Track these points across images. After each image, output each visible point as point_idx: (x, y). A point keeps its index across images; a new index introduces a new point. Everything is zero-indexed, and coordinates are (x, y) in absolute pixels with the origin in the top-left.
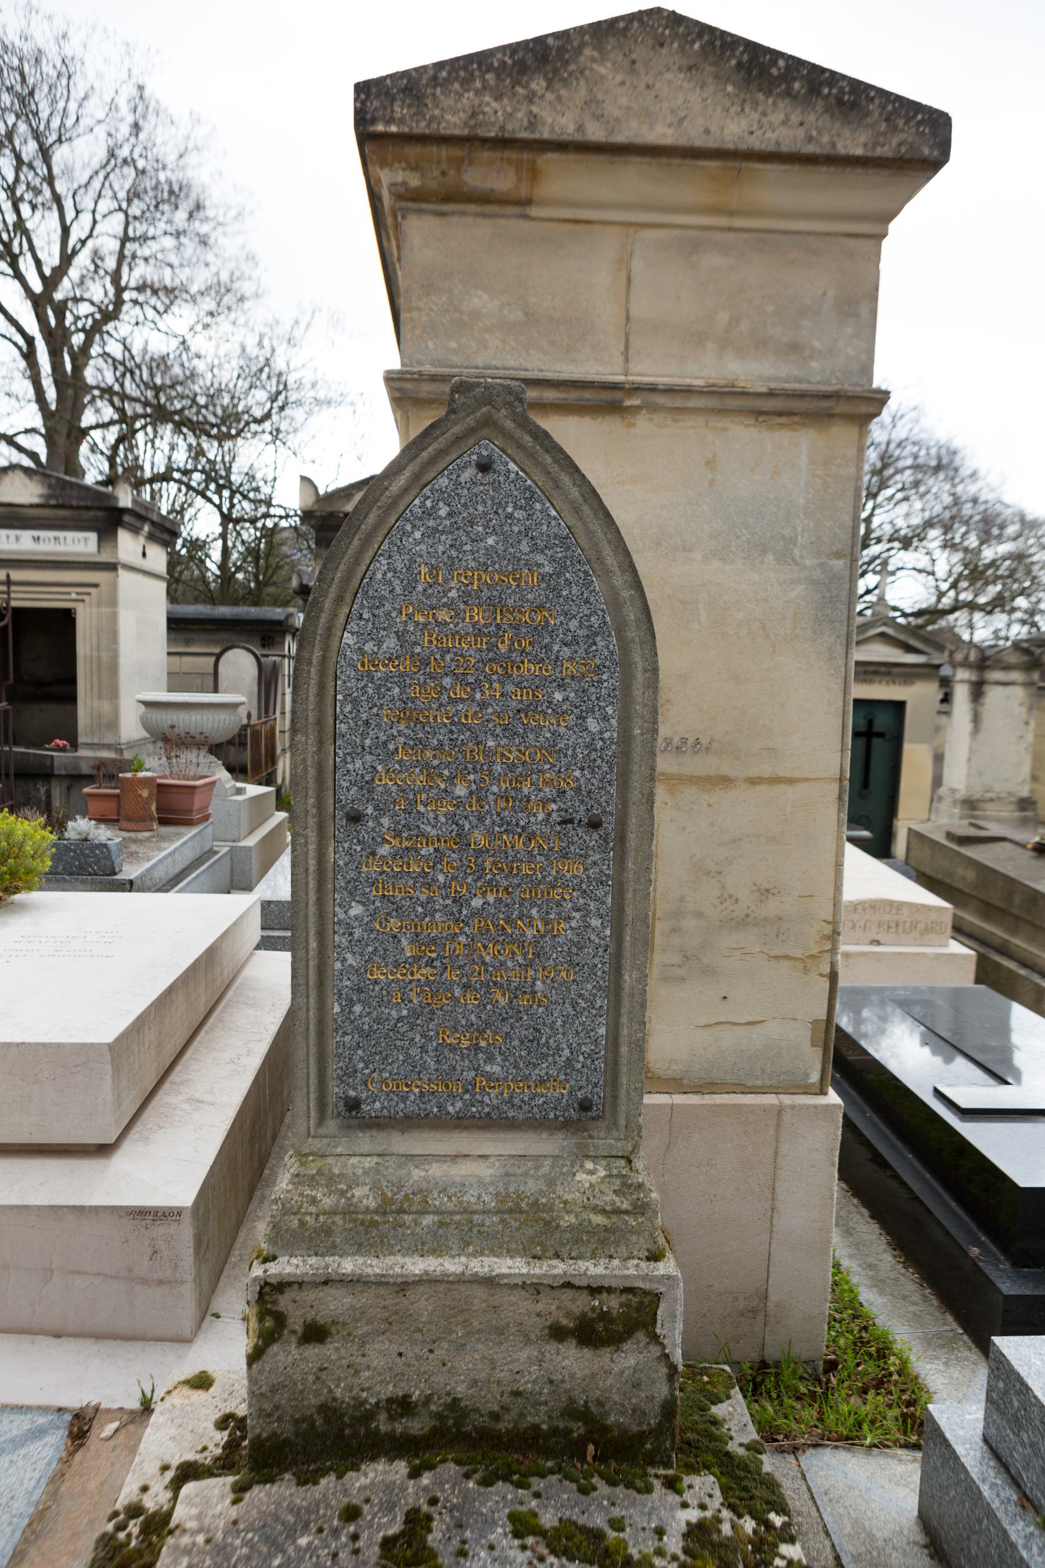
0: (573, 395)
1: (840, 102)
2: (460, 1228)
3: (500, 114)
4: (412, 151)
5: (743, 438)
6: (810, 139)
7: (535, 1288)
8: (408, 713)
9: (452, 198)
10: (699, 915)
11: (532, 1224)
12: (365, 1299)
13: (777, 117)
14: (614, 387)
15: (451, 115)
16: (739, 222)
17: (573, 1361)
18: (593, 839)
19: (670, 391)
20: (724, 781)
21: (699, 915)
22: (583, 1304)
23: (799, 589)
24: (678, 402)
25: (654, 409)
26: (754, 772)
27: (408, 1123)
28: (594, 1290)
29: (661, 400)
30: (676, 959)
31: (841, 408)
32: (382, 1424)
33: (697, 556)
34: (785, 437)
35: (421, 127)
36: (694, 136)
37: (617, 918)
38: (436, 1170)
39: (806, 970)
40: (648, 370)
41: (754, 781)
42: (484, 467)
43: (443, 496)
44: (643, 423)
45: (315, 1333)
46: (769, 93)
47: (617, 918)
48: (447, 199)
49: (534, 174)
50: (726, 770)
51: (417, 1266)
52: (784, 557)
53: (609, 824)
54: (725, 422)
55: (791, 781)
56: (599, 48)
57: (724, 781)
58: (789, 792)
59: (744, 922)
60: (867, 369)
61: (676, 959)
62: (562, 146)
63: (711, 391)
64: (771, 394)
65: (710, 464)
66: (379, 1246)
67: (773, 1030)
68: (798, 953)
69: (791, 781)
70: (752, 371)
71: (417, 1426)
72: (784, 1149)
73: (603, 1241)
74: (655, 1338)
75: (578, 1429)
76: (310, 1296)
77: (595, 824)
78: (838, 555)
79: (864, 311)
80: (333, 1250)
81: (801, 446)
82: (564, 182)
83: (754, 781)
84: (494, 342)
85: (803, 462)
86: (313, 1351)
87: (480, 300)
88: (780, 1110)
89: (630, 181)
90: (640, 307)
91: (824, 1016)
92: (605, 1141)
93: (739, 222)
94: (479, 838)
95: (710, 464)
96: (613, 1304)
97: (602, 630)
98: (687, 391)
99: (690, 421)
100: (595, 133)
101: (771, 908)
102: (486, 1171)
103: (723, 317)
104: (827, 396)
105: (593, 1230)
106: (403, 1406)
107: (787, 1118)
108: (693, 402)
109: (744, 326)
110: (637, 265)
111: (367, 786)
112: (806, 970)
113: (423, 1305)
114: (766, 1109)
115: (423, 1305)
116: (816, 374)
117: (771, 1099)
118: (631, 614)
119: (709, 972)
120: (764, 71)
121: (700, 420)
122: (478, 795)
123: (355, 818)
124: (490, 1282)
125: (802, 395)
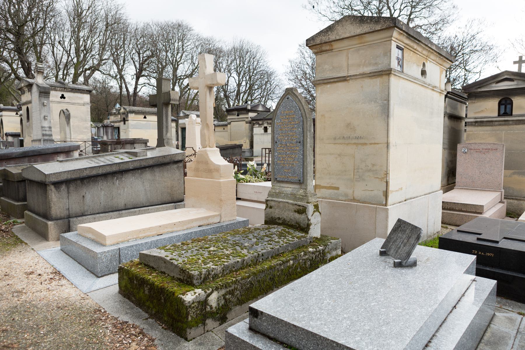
0: (339, 79)
1: (376, 21)
2: (286, 196)
3: (324, 39)
4: (314, 47)
5: (368, 82)
6: (371, 29)
7: (293, 204)
8: (281, 130)
9: (322, 52)
10: (362, 169)
11: (293, 196)
12: (276, 203)
13: (365, 27)
14: (345, 77)
15: (318, 41)
16: (365, 44)
17: (297, 215)
18: (299, 144)
19: (353, 76)
20: (366, 144)
21: (362, 169)
22: (298, 207)
23: (378, 107)
24: (355, 77)
25: (352, 79)
26: (371, 142)
27: (282, 182)
28: (299, 206)
29: (352, 77)
30: (358, 177)
31: (384, 73)
32: (277, 221)
33: (360, 103)
34: (375, 80)
35: (314, 44)
36: (352, 34)
37: (303, 155)
38: (285, 189)
39: (381, 181)
40: (351, 73)
41: (371, 144)
42: (288, 98)
43: (284, 103)
44: (351, 82)
45: (271, 207)
46: (364, 23)
47: (303, 155)
48: (321, 52)
49: (332, 46)
50: (366, 142)
51: (281, 200)
52: (375, 102)
53: (302, 142)
54: (364, 79)
55: (378, 144)
56: (338, 25)
57: (366, 144)
58: (377, 146)
59: (370, 171)
60: (389, 64)
61: (358, 177)
62: (334, 41)
63: (360, 75)
64: (370, 73)
65: (362, 87)
66: (278, 198)
67: (376, 192)
68: (380, 177)
69: (378, 144)
70: (368, 70)
71: (281, 222)
72: (377, 216)
73: (301, 200)
74: (306, 214)
75: (298, 226)
76: (270, 202)
77: (300, 142)
78: (385, 100)
79: (389, 54)
80: (274, 197)
81: (378, 81)
82: (336, 45)
83: (371, 144)
84: (328, 73)
85: (378, 84)
86: (271, 210)
87: (327, 67)
88: (376, 208)
89: (346, 43)
90: (350, 62)
91: (385, 190)
92: (304, 187)
93: (365, 44)
94: (288, 145)
95: (362, 87)
96: (301, 208)
97: (300, 117)
98: (356, 75)
99: (358, 80)
100: (338, 38)
101: (375, 168)
102: (290, 189)
103: (363, 61)
104: (380, 71)
105: (301, 198)
106: (279, 218)
107: (378, 209)
108: (358, 77)
109: (367, 62)
110: (349, 55)
111: (277, 138)
112: (381, 181)
113: (281, 205)
114: (373, 207)
115: (281, 205)
116: (380, 68)
117: (375, 206)
118: (304, 115)
119: (364, 180)
120: (363, 20)
121: (360, 80)
122: (288, 139)
123: (276, 142)
124: (287, 202)
125: (376, 72)
